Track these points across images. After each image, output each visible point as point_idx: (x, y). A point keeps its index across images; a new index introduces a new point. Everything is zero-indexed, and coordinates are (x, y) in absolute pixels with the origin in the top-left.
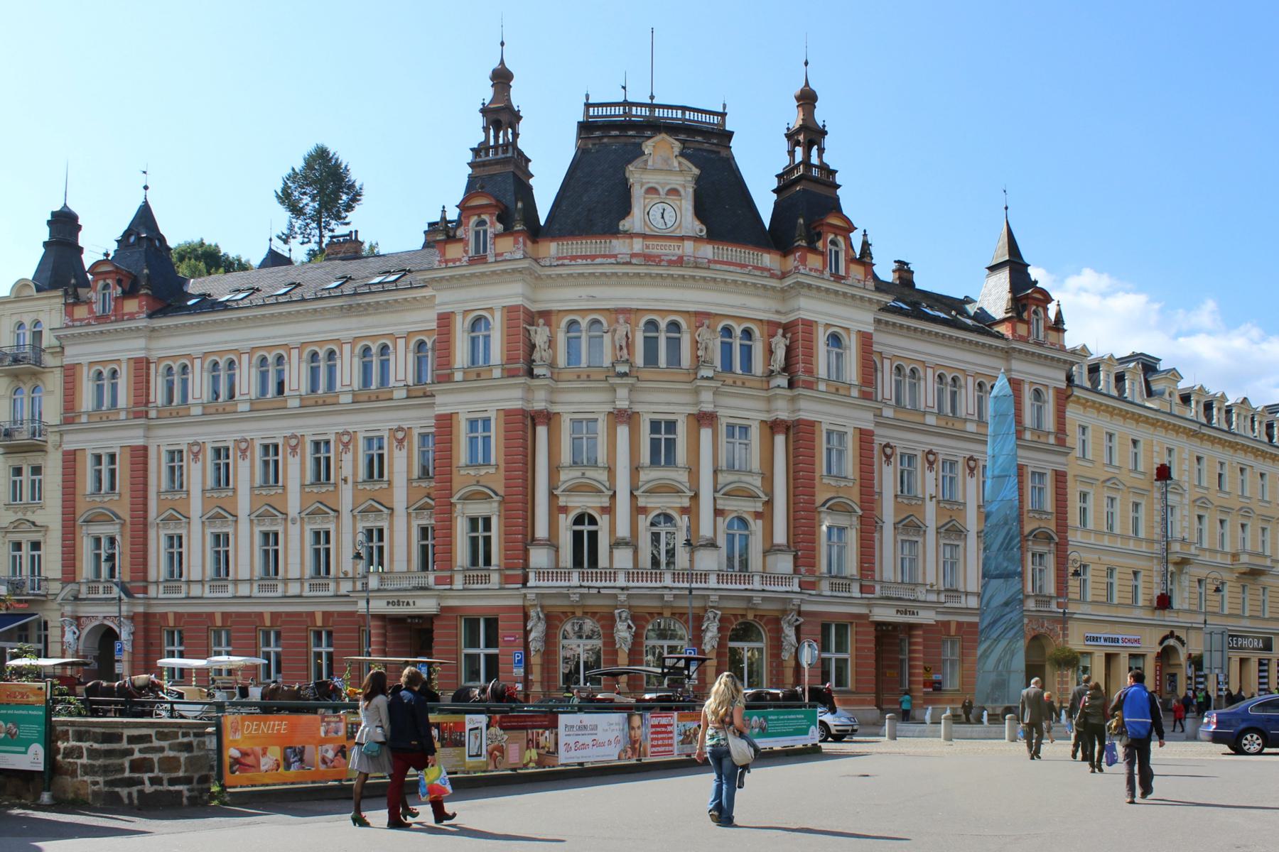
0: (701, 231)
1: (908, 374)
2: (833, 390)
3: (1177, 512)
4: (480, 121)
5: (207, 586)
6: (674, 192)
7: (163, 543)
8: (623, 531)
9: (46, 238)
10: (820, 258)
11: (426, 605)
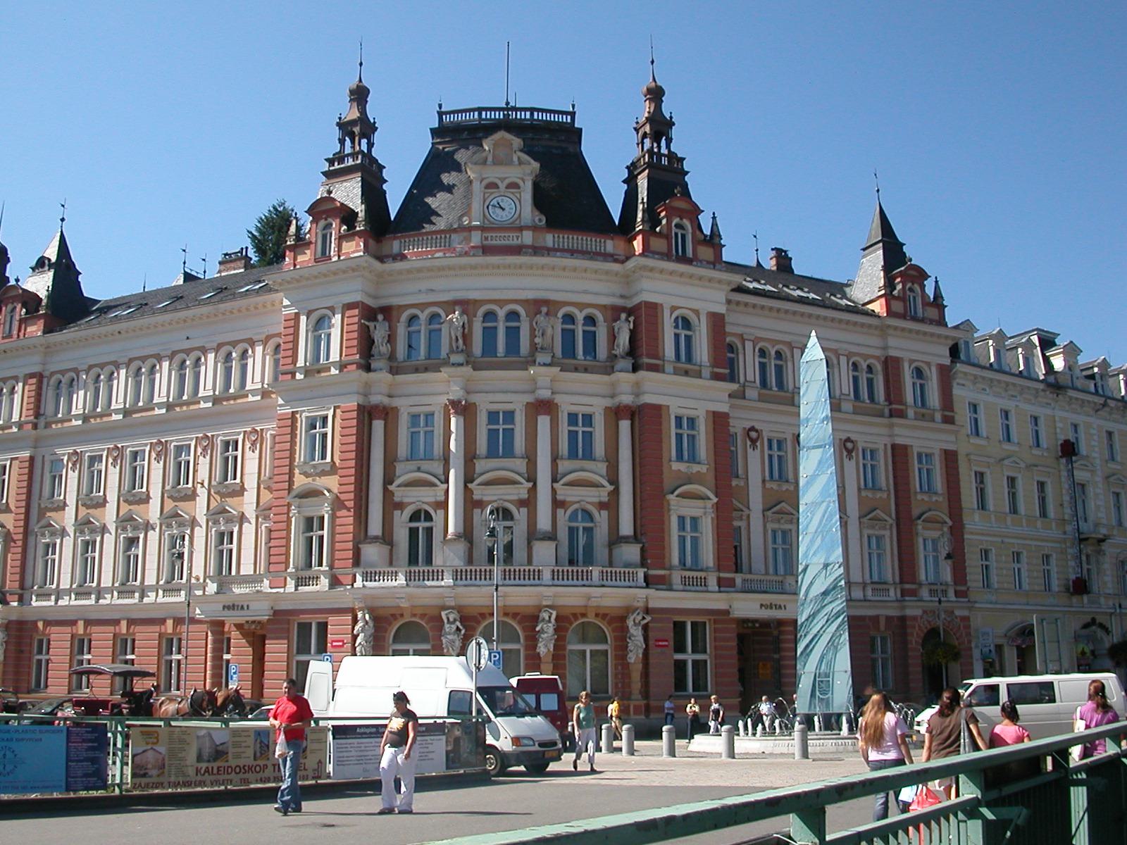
3: (1091, 491)
6: (513, 185)
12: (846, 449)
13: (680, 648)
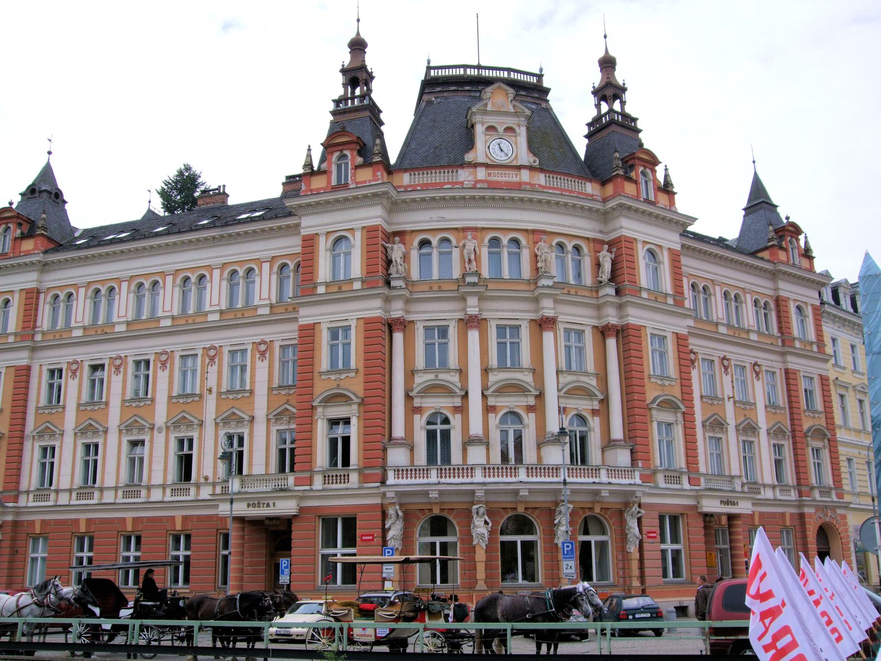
0: (535, 162)
4: (340, 79)
5: (74, 495)
6: (509, 129)
7: (37, 453)
11: (286, 507)
12: (724, 366)
13: (663, 541)
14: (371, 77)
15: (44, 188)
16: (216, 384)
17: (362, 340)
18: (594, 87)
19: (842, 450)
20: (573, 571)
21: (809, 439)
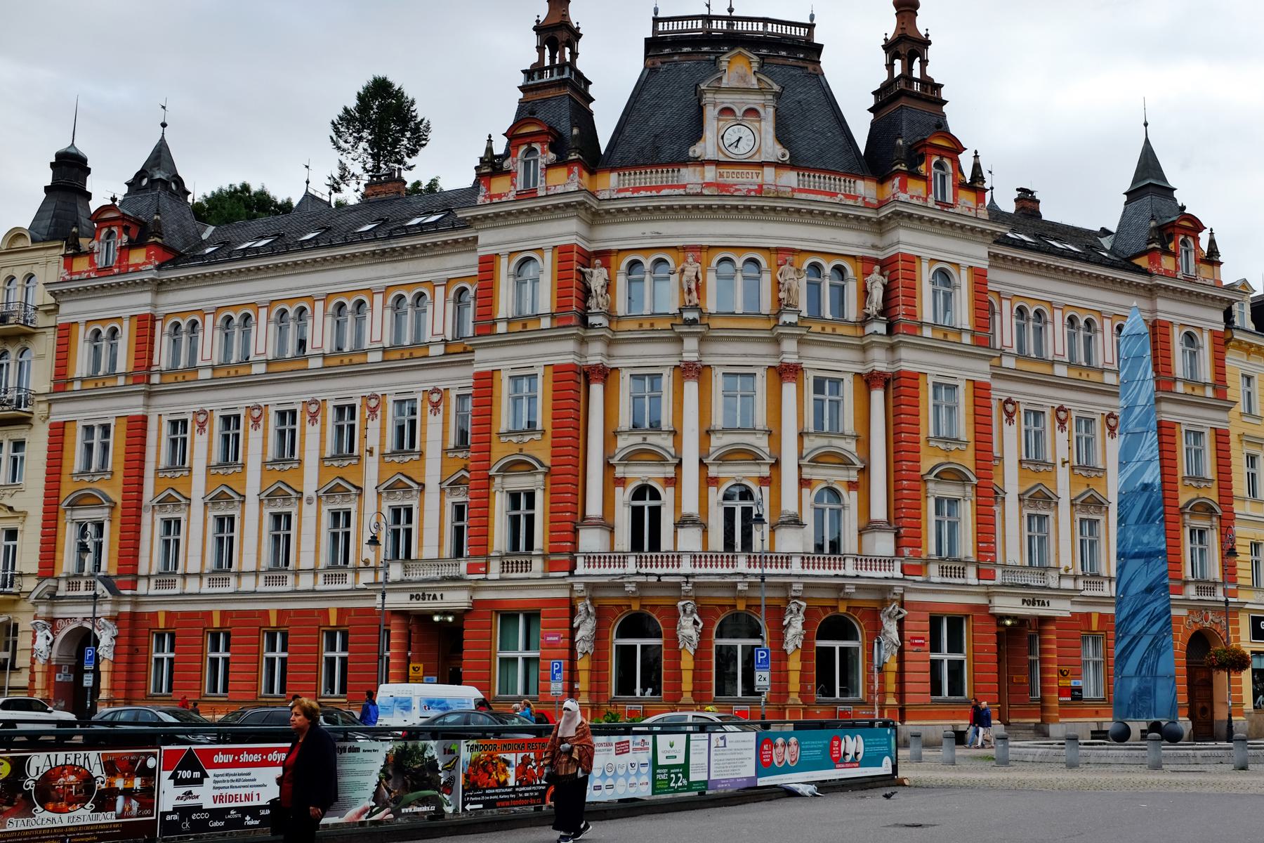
0: (784, 156)
1: (1032, 317)
2: (941, 336)
4: (533, 39)
6: (752, 112)
7: (159, 528)
8: (690, 506)
9: (48, 181)
10: (923, 184)
11: (457, 599)
14: (576, 35)
15: (157, 176)
16: (377, 442)
17: (550, 393)
18: (886, 40)
19: (1239, 530)
20: (767, 683)
21: (1187, 517)
